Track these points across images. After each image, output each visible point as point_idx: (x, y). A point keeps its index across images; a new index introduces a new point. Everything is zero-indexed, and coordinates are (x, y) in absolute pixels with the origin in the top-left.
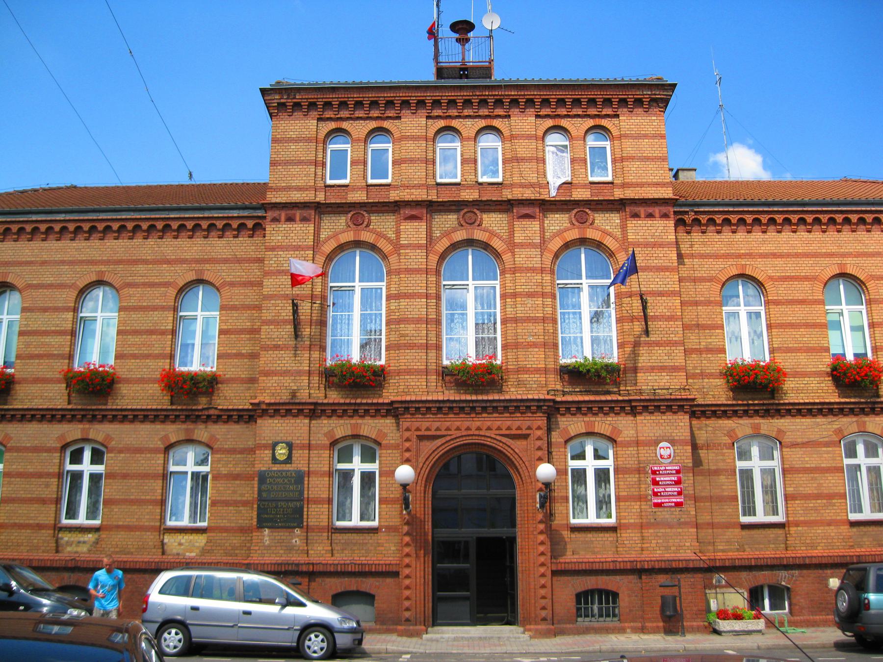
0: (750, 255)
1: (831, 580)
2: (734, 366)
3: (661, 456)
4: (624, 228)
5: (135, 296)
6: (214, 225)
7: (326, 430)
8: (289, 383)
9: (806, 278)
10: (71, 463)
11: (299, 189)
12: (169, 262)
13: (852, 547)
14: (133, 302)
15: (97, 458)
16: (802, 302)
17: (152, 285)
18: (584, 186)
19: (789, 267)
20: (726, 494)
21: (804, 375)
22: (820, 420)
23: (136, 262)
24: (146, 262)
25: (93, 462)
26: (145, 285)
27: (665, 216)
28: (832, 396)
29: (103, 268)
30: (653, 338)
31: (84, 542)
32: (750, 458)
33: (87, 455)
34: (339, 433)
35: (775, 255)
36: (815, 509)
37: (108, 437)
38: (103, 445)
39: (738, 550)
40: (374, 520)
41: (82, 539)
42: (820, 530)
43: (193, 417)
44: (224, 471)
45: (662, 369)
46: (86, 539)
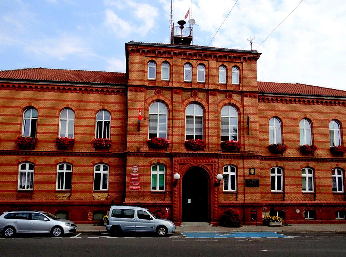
0: (278, 110)
1: (297, 210)
3: (134, 170)
4: (242, 100)
5: (81, 113)
6: (108, 90)
8: (137, 145)
9: (294, 119)
11: (139, 80)
12: (92, 102)
13: (303, 201)
14: (80, 115)
16: (293, 126)
17: (87, 110)
18: (160, 82)
20: (267, 183)
21: (292, 148)
25: (104, 170)
26: (84, 110)
27: (255, 97)
28: (268, 155)
29: (68, 103)
30: (250, 136)
31: (65, 196)
33: (27, 166)
34: (153, 162)
36: (293, 189)
37: (73, 162)
38: (33, 163)
39: (270, 200)
41: (64, 195)
42: (294, 195)
43: (102, 156)
44: (114, 173)
45: (252, 145)
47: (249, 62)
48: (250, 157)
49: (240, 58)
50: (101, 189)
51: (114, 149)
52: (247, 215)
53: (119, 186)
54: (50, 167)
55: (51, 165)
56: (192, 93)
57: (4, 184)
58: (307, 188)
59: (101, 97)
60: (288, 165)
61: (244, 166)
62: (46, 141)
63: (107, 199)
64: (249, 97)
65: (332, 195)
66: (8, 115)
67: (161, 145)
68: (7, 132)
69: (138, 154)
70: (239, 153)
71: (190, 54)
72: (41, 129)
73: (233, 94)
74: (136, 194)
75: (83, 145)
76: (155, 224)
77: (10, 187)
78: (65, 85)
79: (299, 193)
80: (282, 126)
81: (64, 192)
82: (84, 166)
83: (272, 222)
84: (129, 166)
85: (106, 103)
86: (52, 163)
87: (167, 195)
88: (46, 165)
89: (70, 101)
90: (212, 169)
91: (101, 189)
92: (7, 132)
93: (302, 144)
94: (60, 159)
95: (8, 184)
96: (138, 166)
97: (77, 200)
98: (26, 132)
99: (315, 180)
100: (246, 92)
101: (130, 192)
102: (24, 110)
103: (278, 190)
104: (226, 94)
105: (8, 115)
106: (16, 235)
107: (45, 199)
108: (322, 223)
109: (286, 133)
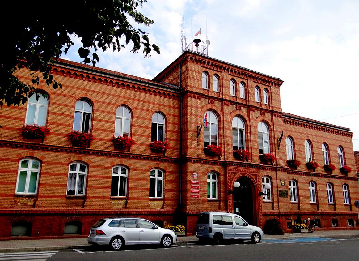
2: (28, 127)
7: (206, 168)
8: (196, 152)
10: (71, 170)
15: (82, 169)
17: (144, 110)
19: (105, 99)
22: (305, 176)
23: (138, 100)
24: (141, 101)
25: (158, 176)
30: (279, 150)
31: (120, 204)
32: (33, 167)
35: (296, 132)
40: (124, 195)
41: (119, 203)
43: (160, 160)
46: (121, 203)
47: (195, 62)
48: (161, 159)
49: (269, 82)
50: (156, 197)
51: (170, 153)
52: (297, 221)
53: (174, 193)
54: (105, 169)
55: (107, 168)
56: (210, 100)
57: (52, 187)
58: (211, 196)
59: (157, 99)
60: (49, 156)
61: (277, 177)
62: (101, 139)
63: (163, 207)
64: (193, 98)
65: (328, 206)
66: (59, 104)
67: (218, 153)
68: (58, 124)
69: (197, 160)
70: (273, 165)
71: (260, 79)
72: (97, 125)
73: (266, 112)
74: (196, 202)
75: (140, 147)
76: (251, 230)
77: (59, 191)
78: (122, 80)
79: (308, 204)
80: (132, 117)
81: (120, 199)
82: (142, 170)
83: (302, 229)
84: (190, 172)
85: (162, 105)
86: (108, 165)
87: (222, 204)
88: (102, 167)
89: (127, 98)
90: (256, 179)
91: (156, 197)
92: (58, 124)
93: (27, 122)
94: (74, 157)
95: (57, 187)
96: (197, 173)
97: (134, 208)
98: (78, 127)
99: (129, 181)
100: (275, 112)
101: (192, 200)
102: (77, 100)
103: (158, 196)
104: (209, 99)
105: (59, 104)
106: (125, 247)
107: (99, 206)
108: (324, 230)
109: (96, 120)
